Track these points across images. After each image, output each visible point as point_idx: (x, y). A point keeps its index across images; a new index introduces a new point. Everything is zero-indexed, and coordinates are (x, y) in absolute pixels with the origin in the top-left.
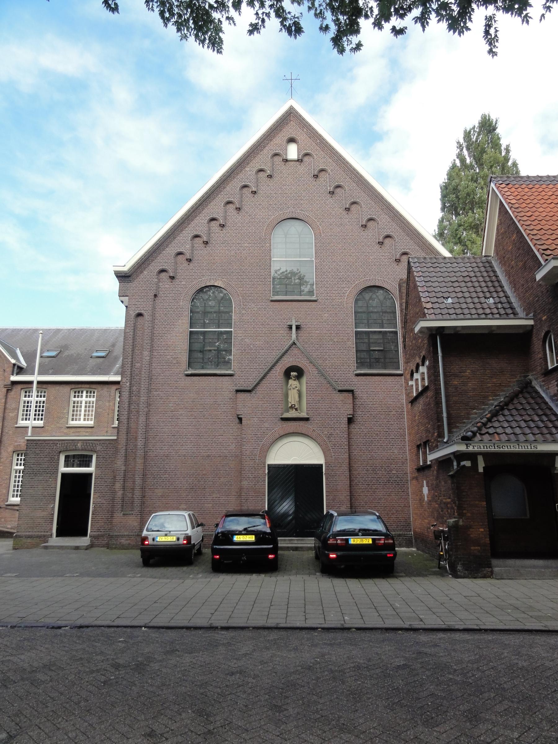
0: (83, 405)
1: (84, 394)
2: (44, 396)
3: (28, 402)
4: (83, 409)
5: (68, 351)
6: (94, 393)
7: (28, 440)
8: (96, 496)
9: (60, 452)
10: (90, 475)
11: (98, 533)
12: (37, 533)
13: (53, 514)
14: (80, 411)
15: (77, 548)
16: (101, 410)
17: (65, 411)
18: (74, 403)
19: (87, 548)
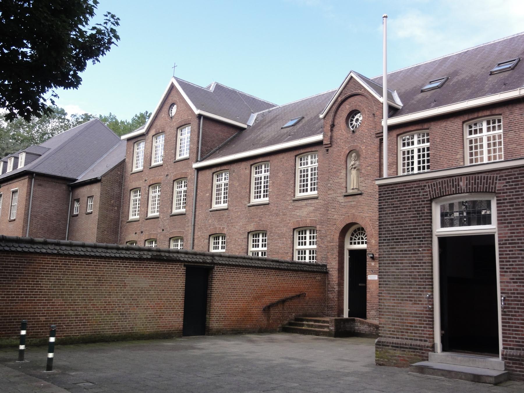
0: (485, 143)
1: (485, 126)
2: (428, 141)
3: (408, 152)
4: (485, 149)
5: (457, 77)
6: (499, 121)
7: (380, 186)
8: (506, 279)
9: (431, 200)
10: (491, 237)
11: (518, 353)
12: (409, 342)
13: (432, 310)
14: (482, 153)
15: (477, 379)
16: (514, 146)
17: (458, 156)
18: (471, 142)
19: (498, 381)
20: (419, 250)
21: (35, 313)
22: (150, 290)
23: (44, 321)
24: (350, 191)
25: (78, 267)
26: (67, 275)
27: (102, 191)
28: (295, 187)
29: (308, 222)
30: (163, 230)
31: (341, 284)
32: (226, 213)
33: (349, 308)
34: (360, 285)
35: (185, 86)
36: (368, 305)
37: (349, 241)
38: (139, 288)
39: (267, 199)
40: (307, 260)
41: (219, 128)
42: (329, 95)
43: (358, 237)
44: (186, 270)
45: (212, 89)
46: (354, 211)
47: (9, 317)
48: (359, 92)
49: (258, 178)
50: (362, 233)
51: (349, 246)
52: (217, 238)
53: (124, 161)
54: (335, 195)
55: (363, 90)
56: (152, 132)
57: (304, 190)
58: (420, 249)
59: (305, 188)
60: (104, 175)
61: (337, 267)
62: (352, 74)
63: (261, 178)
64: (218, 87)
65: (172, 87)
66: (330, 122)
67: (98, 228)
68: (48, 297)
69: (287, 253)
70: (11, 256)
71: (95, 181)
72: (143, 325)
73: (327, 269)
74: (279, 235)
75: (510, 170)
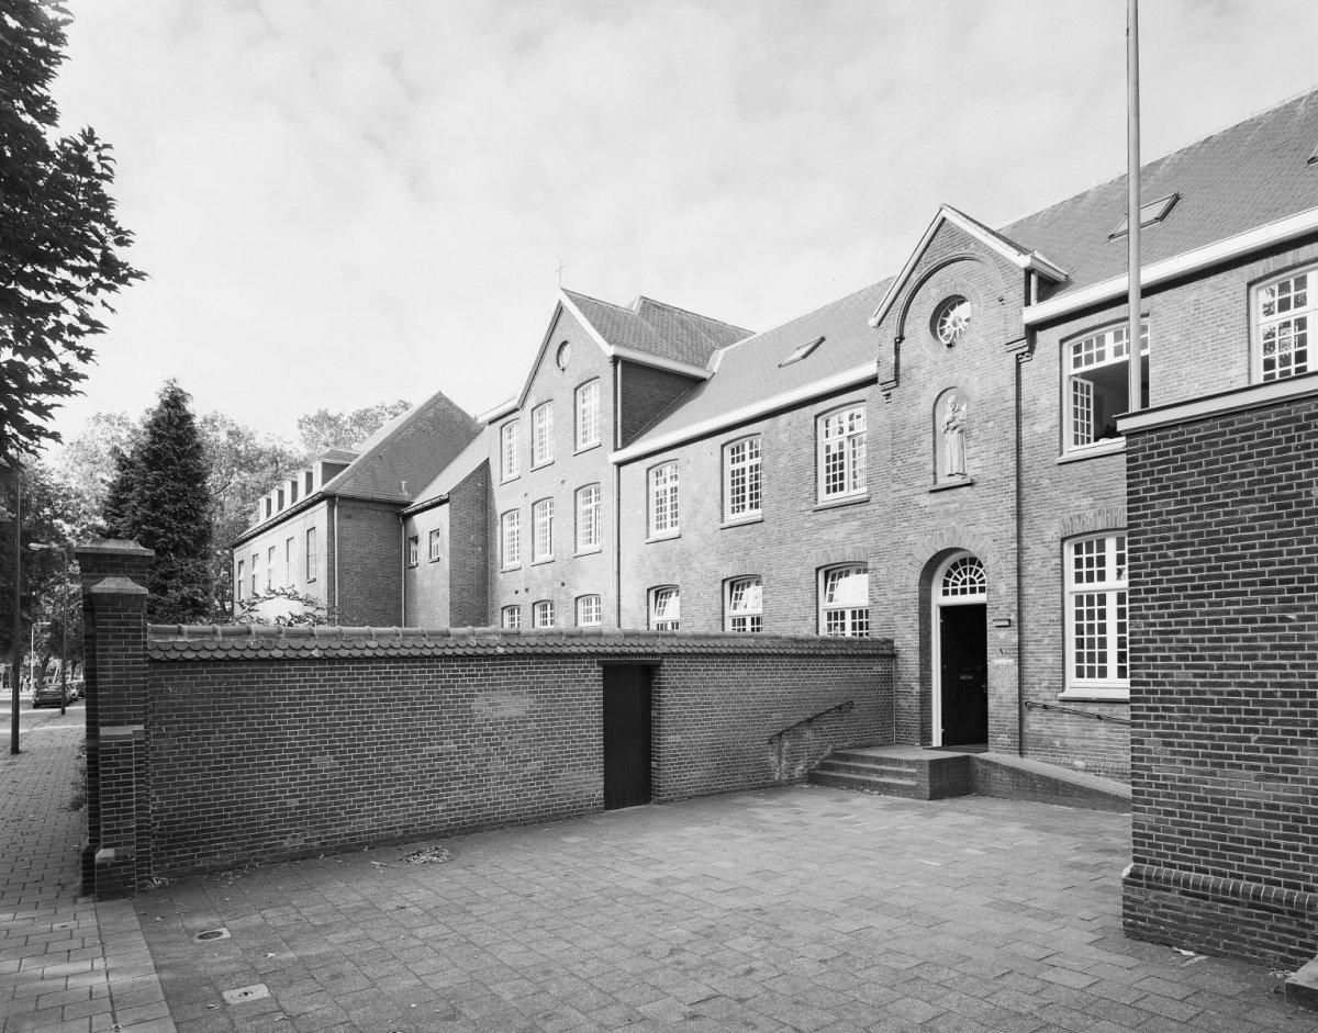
20: (1283, 619)
21: (275, 792)
22: (530, 722)
23: (296, 808)
24: (943, 481)
25: (362, 685)
26: (339, 703)
27: (452, 518)
28: (816, 481)
29: (848, 554)
30: (563, 584)
31: (925, 679)
33: (943, 726)
34: (962, 678)
35: (584, 304)
36: (991, 722)
37: (941, 588)
38: (504, 718)
39: (759, 511)
40: (848, 633)
42: (871, 293)
43: (961, 580)
44: (604, 671)
45: (636, 308)
46: (954, 524)
47: (215, 805)
48: (964, 251)
49: (738, 471)
50: (971, 569)
51: (939, 599)
54: (907, 492)
55: (972, 246)
56: (531, 402)
57: (835, 487)
58: (1292, 616)
59: (838, 482)
61: (916, 643)
62: (944, 213)
63: (743, 470)
64: (649, 306)
65: (560, 310)
66: (893, 333)
68: (301, 755)
69: (805, 619)
70: (202, 672)
72: (518, 796)
73: (893, 648)
75: (1286, 408)
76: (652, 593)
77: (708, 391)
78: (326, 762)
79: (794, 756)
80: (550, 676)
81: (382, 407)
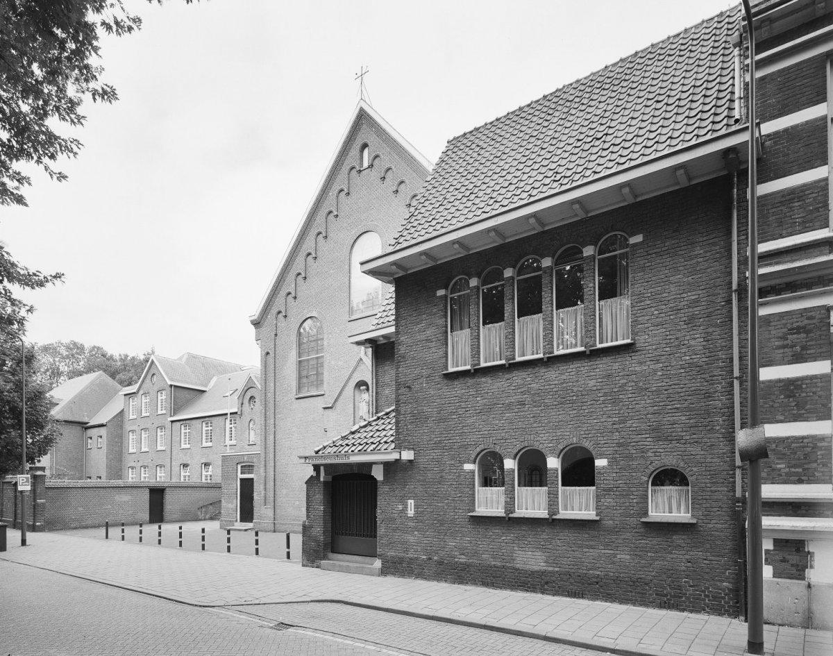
2: (211, 426)
24: (251, 443)
32: (189, 451)
41: (186, 392)
52: (145, 468)
53: (123, 410)
60: (109, 421)
67: (740, 369)
71: (102, 425)
74: (813, 393)
76: (203, 465)
77: (206, 395)
78: (81, 509)
79: (206, 513)
80: (135, 491)
81: (59, 342)
